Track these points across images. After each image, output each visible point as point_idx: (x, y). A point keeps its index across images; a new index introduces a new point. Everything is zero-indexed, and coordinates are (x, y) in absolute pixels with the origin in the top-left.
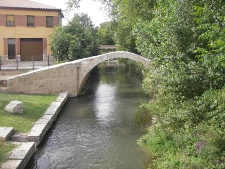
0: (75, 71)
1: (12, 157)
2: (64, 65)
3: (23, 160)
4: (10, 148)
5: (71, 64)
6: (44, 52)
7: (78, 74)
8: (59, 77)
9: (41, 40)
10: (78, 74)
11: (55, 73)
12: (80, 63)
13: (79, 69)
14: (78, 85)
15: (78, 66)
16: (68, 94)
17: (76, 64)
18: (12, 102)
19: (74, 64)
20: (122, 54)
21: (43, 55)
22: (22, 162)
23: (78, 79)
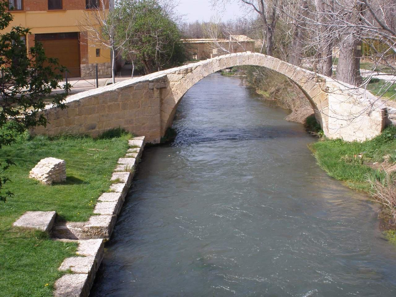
0: (156, 94)
1: (78, 253)
2: (135, 84)
3: (90, 274)
4: (276, 31)
5: (148, 81)
6: (84, 60)
7: (161, 100)
8: (124, 107)
9: (74, 36)
10: (161, 100)
11: (116, 100)
12: (164, 80)
13: (164, 91)
14: (162, 121)
15: (162, 85)
16: (144, 140)
17: (157, 80)
18: (43, 161)
19: (152, 81)
20: (249, 57)
21: (82, 66)
22: (88, 277)
23: (161, 111)
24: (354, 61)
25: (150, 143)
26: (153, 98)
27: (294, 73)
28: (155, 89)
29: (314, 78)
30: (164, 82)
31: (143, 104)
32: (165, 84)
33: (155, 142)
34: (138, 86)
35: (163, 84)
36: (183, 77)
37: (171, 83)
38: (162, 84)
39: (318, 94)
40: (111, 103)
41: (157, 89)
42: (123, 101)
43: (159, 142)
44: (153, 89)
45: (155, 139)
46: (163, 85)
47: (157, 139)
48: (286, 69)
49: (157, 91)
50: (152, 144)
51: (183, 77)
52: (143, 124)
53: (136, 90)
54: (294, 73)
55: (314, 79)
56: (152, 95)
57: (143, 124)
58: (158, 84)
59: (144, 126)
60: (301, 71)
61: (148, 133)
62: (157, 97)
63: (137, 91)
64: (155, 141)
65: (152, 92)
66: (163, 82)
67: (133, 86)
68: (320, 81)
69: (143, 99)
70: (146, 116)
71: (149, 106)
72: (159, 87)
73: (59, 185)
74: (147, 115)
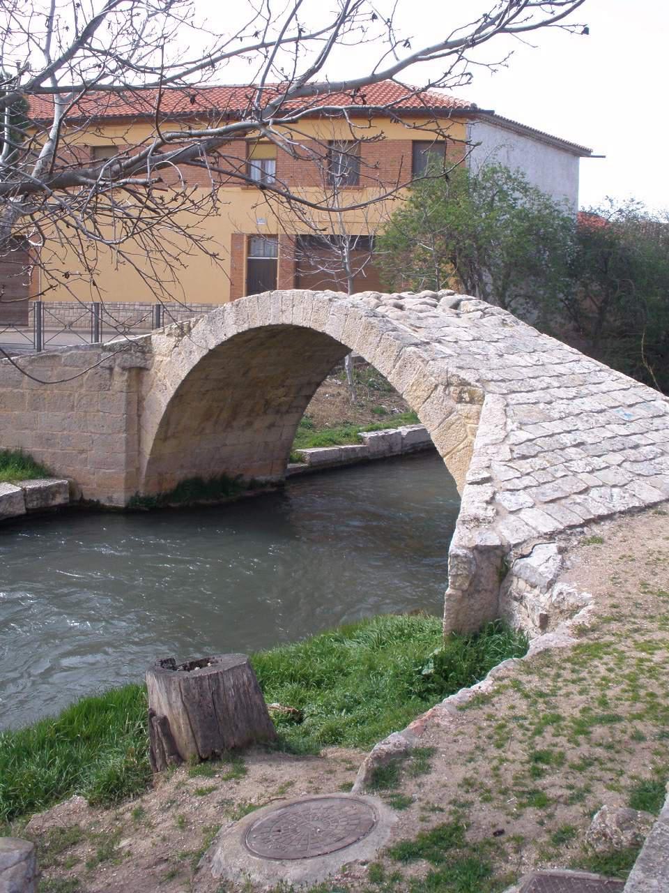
0: (120, 381)
24: (633, 253)
25: (98, 501)
26: (109, 390)
27: (396, 361)
28: (117, 369)
29: (452, 384)
30: (144, 353)
31: (84, 402)
32: (146, 360)
33: (111, 501)
34: (71, 356)
35: (139, 360)
36: (175, 346)
37: (158, 358)
38: (137, 357)
39: (461, 446)
40: (4, 390)
41: (124, 369)
42: (32, 390)
43: (122, 505)
44: (111, 369)
45: (110, 495)
46: (138, 362)
47: (115, 496)
48: (378, 346)
49: (122, 374)
50: (103, 505)
51: (175, 346)
52: (82, 452)
53: (66, 366)
54: (396, 361)
55: (452, 389)
56: (108, 383)
57: (82, 452)
58: (125, 356)
59: (84, 456)
60: (414, 356)
61: (92, 477)
62: (119, 389)
63: (67, 368)
64: (110, 499)
65: (108, 376)
66: (138, 354)
67: (58, 356)
68: (466, 396)
69: (83, 391)
70: (89, 434)
71: (98, 411)
72: (127, 365)
73: (319, 462)
74: (93, 431)
